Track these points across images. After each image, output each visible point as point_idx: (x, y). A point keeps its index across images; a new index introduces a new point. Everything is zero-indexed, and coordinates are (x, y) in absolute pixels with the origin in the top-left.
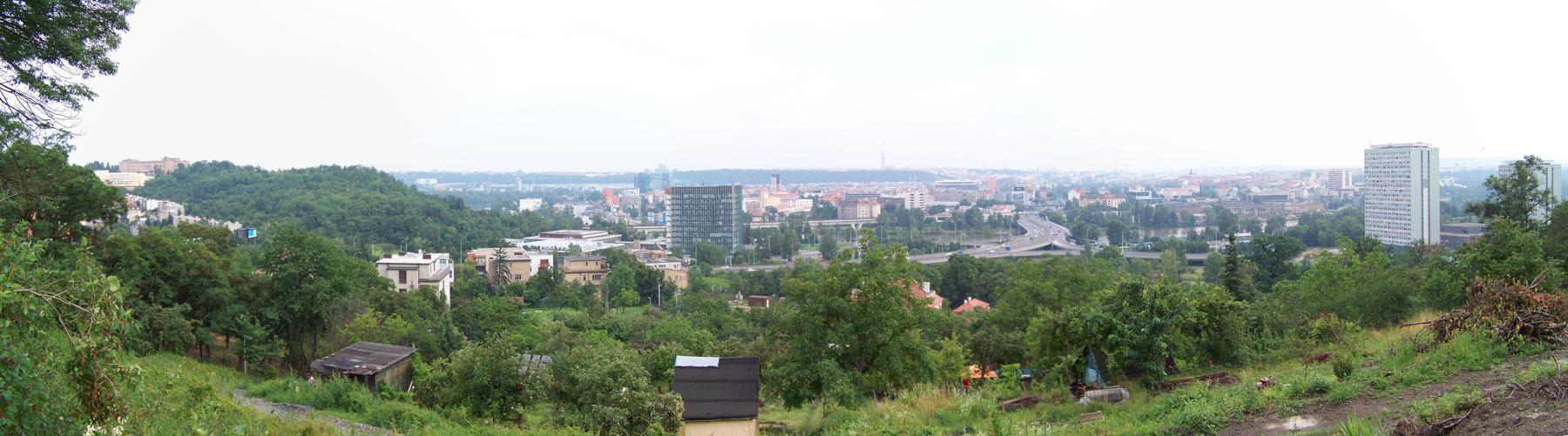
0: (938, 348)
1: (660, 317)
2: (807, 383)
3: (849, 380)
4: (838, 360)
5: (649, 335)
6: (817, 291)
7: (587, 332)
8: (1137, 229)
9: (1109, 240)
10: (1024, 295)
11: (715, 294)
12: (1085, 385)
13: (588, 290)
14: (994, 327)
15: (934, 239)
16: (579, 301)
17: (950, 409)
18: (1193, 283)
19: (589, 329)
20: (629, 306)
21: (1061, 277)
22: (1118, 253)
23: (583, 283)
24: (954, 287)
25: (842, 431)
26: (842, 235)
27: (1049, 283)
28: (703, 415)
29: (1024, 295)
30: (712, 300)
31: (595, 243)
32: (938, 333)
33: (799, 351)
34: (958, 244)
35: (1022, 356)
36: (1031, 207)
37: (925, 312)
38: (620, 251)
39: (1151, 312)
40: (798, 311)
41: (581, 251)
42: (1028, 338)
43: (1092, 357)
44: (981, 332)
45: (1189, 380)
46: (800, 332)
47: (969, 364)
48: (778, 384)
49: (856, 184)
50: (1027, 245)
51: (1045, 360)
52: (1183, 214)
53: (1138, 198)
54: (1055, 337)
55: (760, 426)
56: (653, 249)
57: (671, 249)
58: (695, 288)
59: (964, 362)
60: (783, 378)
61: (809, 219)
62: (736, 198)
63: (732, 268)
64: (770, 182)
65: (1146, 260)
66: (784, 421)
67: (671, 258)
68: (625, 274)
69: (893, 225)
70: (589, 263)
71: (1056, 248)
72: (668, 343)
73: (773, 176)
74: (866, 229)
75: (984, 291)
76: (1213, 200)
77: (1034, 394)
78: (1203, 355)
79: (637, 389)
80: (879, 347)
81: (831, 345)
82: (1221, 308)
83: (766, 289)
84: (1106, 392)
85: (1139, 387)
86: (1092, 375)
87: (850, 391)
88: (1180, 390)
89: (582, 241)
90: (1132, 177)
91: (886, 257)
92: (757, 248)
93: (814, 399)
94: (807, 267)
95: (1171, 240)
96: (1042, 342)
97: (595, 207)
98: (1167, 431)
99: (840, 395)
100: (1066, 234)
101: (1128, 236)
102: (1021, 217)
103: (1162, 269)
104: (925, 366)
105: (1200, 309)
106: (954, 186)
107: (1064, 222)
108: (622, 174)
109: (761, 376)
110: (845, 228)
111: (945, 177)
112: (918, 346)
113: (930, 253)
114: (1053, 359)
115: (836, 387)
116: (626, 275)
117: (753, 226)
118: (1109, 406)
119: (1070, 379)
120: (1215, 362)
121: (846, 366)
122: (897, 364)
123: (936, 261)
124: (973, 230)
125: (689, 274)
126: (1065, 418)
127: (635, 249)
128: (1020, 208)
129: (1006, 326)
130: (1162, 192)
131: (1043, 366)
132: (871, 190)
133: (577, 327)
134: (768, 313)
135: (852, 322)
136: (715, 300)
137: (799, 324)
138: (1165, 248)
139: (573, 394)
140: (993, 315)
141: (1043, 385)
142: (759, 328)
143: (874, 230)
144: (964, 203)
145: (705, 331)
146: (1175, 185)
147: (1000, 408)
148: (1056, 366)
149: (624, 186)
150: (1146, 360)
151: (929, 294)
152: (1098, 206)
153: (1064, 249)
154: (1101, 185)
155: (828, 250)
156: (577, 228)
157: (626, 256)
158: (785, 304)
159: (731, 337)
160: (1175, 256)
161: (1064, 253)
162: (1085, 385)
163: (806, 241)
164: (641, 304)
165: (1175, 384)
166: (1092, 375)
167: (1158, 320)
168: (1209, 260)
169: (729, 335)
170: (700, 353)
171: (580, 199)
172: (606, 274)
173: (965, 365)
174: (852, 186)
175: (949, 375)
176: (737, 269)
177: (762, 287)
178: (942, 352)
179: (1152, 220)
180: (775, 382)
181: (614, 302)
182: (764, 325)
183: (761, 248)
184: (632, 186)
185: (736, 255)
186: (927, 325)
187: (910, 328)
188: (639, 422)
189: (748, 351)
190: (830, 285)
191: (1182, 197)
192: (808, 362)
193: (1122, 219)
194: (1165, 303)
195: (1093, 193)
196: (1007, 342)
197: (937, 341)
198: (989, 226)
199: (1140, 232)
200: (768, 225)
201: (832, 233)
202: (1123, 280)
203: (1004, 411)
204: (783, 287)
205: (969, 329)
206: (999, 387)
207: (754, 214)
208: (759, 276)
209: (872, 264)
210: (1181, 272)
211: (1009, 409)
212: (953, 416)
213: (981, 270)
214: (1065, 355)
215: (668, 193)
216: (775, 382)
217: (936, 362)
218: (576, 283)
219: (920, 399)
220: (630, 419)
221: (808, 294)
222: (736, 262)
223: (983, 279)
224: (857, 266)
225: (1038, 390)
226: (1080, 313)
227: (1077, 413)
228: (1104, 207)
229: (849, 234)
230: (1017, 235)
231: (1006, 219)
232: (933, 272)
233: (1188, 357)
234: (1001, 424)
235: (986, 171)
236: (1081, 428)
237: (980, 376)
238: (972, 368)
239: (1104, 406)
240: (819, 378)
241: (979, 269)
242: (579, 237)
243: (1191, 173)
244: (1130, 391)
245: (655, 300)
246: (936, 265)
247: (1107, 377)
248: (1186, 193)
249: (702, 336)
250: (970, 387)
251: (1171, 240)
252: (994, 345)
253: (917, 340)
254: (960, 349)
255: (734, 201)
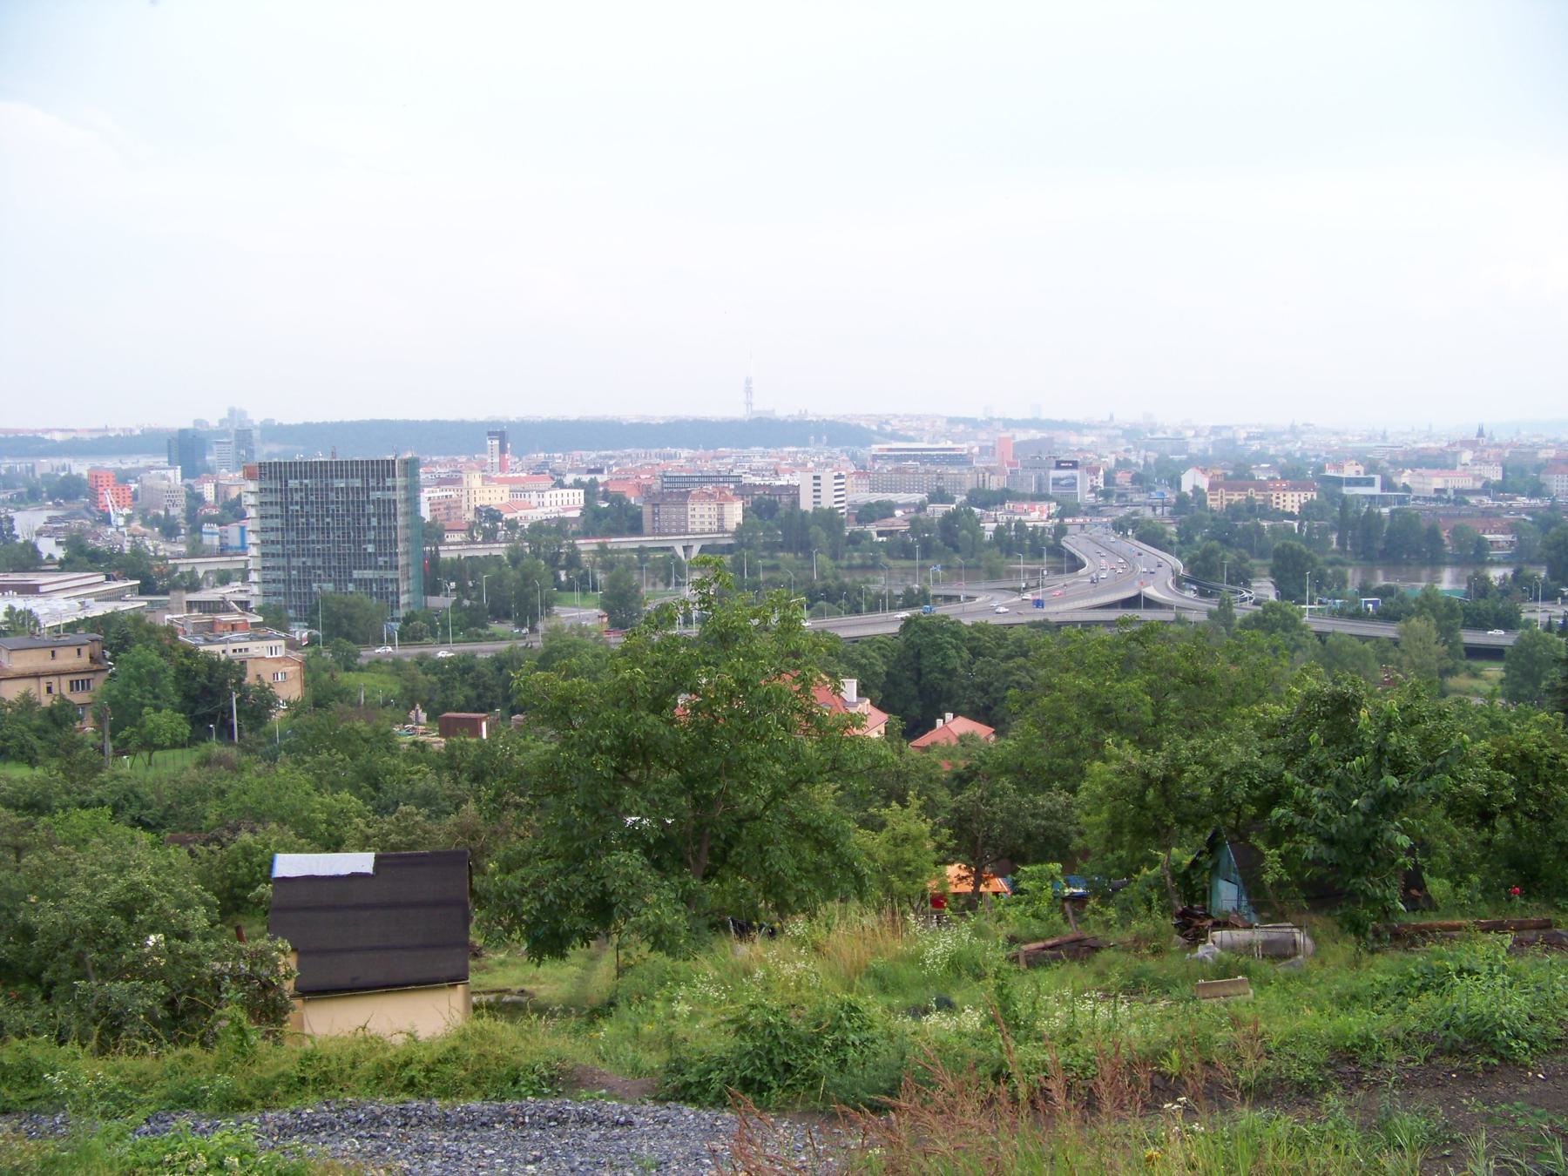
0: (877, 825)
1: (236, 769)
2: (577, 904)
3: (673, 895)
4: (647, 852)
5: (212, 812)
6: (597, 701)
7: (60, 815)
8: (1342, 564)
9: (1277, 587)
10: (1073, 710)
11: (371, 709)
12: (1209, 916)
13: (60, 716)
14: (1005, 781)
15: (868, 581)
16: (36, 743)
17: (901, 958)
18: (1477, 701)
19: (64, 808)
20: (162, 747)
21: (1161, 670)
22: (1295, 620)
23: (46, 701)
24: (914, 691)
25: (658, 1004)
26: (654, 570)
27: (1133, 685)
28: (343, 980)
29: (1073, 710)
30: (360, 725)
31: (75, 602)
32: (876, 792)
33: (559, 835)
34: (923, 592)
35: (1067, 846)
36: (1093, 507)
37: (847, 747)
38: (137, 619)
39: (1378, 762)
40: (553, 747)
41: (37, 623)
42: (1080, 806)
43: (1228, 855)
44: (973, 792)
45: (1458, 928)
46: (560, 792)
47: (945, 862)
48: (514, 908)
49: (685, 453)
50: (1082, 597)
51: (1120, 858)
52: (1456, 532)
53: (1346, 490)
54: (1142, 805)
55: (475, 999)
56: (218, 612)
57: (260, 611)
58: (321, 697)
59: (935, 856)
60: (524, 893)
61: (577, 535)
62: (406, 488)
63: (398, 651)
64: (483, 450)
65: (1364, 639)
66: (527, 988)
67: (262, 632)
68: (150, 672)
69: (773, 547)
70: (59, 652)
71: (1150, 603)
72: (259, 829)
73: (491, 434)
74: (708, 557)
75: (981, 700)
76: (1536, 502)
77: (1094, 931)
78: (1495, 873)
79: (184, 936)
80: (740, 823)
81: (630, 820)
82: (1550, 766)
83: (479, 697)
84: (1258, 935)
85: (1337, 929)
86: (1227, 895)
87: (676, 918)
88: (1436, 947)
89: (40, 601)
90: (1334, 441)
91: (756, 622)
92: (457, 604)
93: (594, 937)
94: (574, 645)
95: (1427, 596)
96: (1113, 815)
97: (71, 516)
98: (1401, 1035)
99: (654, 927)
100: (1174, 572)
101: (1320, 582)
102: (1070, 530)
103: (1398, 662)
104: (845, 864)
105: (1498, 763)
106: (915, 458)
107: (1171, 543)
108: (138, 432)
109: (473, 892)
110: (660, 555)
111: (894, 436)
112: (829, 821)
113: (858, 612)
114: (1138, 855)
115: (644, 910)
116: (154, 676)
117: (447, 554)
118: (1266, 968)
119: (1176, 902)
120: (1527, 895)
121: (666, 864)
122: (782, 861)
123: (870, 631)
124: (958, 559)
125: (306, 666)
126: (1163, 986)
127: (174, 615)
128: (1068, 509)
129: (1030, 778)
130: (1405, 478)
131: (1114, 871)
132: (720, 467)
133: (35, 806)
134: (486, 751)
135: (677, 768)
136: (368, 722)
137: (557, 773)
138: (1410, 613)
139: (31, 964)
140: (1001, 754)
141: (1112, 913)
142: (465, 785)
143: (727, 559)
144: (939, 496)
145: (345, 795)
146: (1439, 461)
147: (1014, 959)
148: (1145, 870)
149: (143, 461)
150: (1357, 872)
151: (854, 705)
152: (1252, 509)
153: (1170, 607)
154: (1260, 457)
155: (620, 606)
156: (24, 569)
157: (152, 630)
158: (523, 729)
159: (402, 808)
160: (1435, 635)
161: (1169, 616)
162: (1209, 916)
163: (569, 587)
164: (192, 742)
165: (1424, 932)
166: (1227, 895)
167: (1393, 782)
168: (1521, 648)
169: (397, 804)
170: (334, 844)
171: (32, 496)
172: (105, 676)
173: (936, 864)
174: (674, 457)
175: (898, 885)
176: (411, 653)
177: (472, 693)
178: (884, 835)
179: (1380, 545)
180: (506, 904)
181: (126, 741)
182: (478, 777)
183: (466, 603)
184: (163, 461)
185: (407, 620)
186: (850, 774)
187: (811, 781)
188: (192, 1008)
189: (442, 837)
190: (629, 687)
191: (1456, 491)
192: (579, 857)
193: (1308, 541)
194: (1411, 743)
195: (1238, 475)
196: (1033, 816)
197: (872, 810)
198: (997, 550)
199: (1350, 572)
200: (481, 551)
201: (629, 566)
202: (1312, 683)
203: (1023, 966)
204: (519, 691)
205: (946, 784)
206: (1013, 912)
207: (447, 525)
208: (463, 668)
209: (723, 638)
210: (1448, 672)
211: (1035, 961)
212: (907, 973)
213: (976, 653)
214: (1166, 848)
215: (250, 475)
216: (506, 904)
217: (870, 856)
218: (28, 703)
219: (833, 937)
220: (170, 1004)
221: (576, 708)
222: (409, 636)
223: (980, 672)
224: (689, 643)
225: (1100, 922)
226: (1208, 755)
227: (1188, 977)
228: (1265, 511)
229: (670, 570)
230: (1059, 571)
231: (1035, 536)
232: (864, 656)
233: (1458, 872)
234: (1015, 994)
235: (990, 422)
236: (1198, 1011)
237: (969, 889)
238: (953, 870)
239: (1252, 965)
240: (605, 893)
241: (973, 651)
242: (33, 590)
243: (1481, 434)
244: (1315, 939)
245: (226, 732)
246: (870, 641)
247: (1262, 903)
248: (1467, 483)
249: (338, 806)
250: (947, 910)
251: (1427, 596)
252: (1002, 821)
253: (828, 808)
254: (926, 828)
255: (399, 495)
